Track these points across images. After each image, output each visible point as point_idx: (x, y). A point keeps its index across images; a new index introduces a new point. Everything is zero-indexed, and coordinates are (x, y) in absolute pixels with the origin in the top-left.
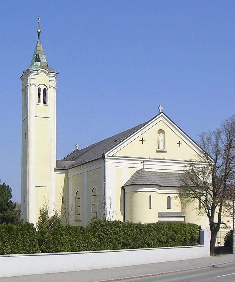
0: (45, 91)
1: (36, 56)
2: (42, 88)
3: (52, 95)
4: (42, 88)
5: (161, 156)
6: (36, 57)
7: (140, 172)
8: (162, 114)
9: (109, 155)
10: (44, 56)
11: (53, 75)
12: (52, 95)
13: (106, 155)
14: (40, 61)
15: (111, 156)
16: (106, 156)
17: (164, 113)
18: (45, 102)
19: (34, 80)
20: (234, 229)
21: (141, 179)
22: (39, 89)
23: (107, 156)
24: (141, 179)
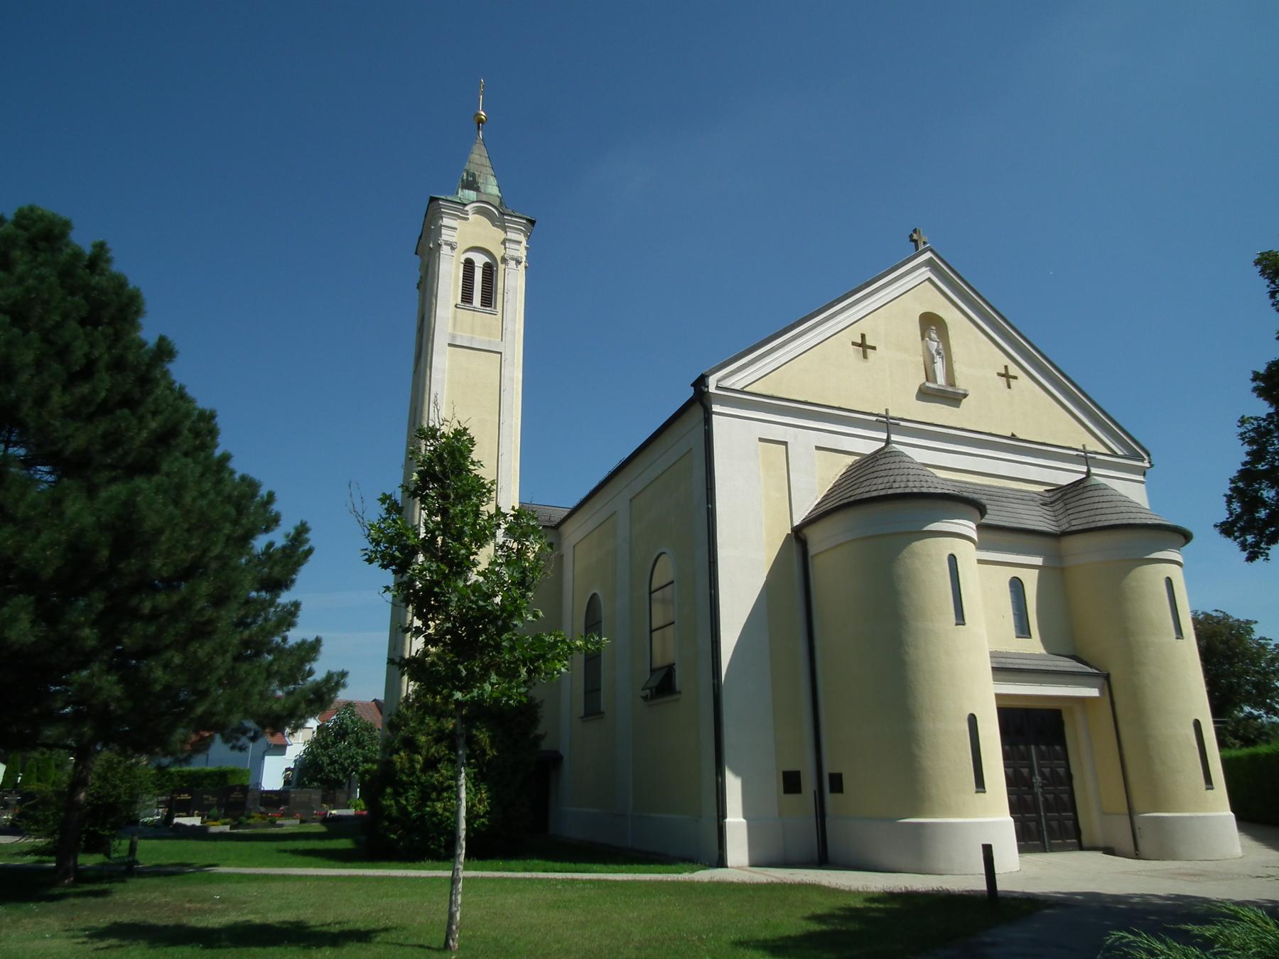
0: (489, 271)
1: (465, 174)
2: (480, 260)
3: (513, 283)
4: (480, 260)
5: (938, 413)
6: (465, 178)
7: (866, 465)
8: (928, 255)
9: (726, 384)
10: (493, 181)
11: (515, 223)
12: (513, 283)
13: (712, 382)
14: (477, 189)
15: (738, 387)
16: (712, 389)
17: (935, 250)
18: (488, 300)
19: (451, 232)
20: (307, 728)
21: (892, 479)
22: (469, 265)
23: (718, 388)
24: (892, 479)
